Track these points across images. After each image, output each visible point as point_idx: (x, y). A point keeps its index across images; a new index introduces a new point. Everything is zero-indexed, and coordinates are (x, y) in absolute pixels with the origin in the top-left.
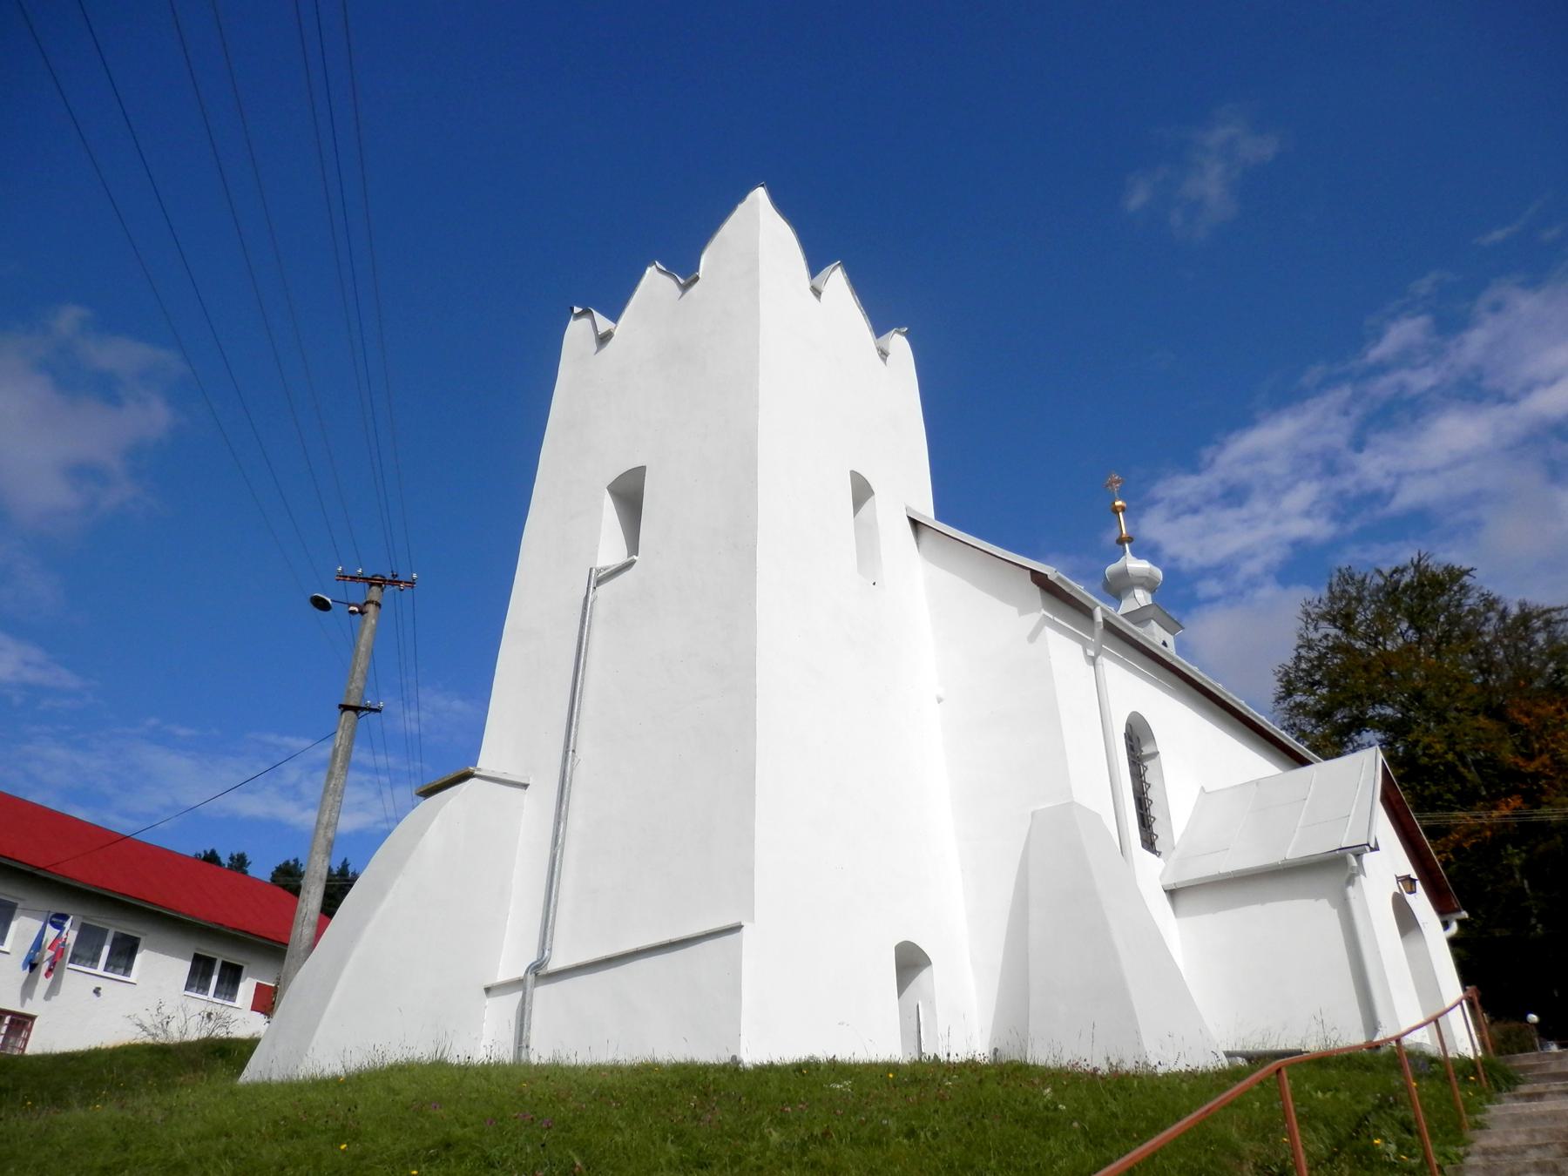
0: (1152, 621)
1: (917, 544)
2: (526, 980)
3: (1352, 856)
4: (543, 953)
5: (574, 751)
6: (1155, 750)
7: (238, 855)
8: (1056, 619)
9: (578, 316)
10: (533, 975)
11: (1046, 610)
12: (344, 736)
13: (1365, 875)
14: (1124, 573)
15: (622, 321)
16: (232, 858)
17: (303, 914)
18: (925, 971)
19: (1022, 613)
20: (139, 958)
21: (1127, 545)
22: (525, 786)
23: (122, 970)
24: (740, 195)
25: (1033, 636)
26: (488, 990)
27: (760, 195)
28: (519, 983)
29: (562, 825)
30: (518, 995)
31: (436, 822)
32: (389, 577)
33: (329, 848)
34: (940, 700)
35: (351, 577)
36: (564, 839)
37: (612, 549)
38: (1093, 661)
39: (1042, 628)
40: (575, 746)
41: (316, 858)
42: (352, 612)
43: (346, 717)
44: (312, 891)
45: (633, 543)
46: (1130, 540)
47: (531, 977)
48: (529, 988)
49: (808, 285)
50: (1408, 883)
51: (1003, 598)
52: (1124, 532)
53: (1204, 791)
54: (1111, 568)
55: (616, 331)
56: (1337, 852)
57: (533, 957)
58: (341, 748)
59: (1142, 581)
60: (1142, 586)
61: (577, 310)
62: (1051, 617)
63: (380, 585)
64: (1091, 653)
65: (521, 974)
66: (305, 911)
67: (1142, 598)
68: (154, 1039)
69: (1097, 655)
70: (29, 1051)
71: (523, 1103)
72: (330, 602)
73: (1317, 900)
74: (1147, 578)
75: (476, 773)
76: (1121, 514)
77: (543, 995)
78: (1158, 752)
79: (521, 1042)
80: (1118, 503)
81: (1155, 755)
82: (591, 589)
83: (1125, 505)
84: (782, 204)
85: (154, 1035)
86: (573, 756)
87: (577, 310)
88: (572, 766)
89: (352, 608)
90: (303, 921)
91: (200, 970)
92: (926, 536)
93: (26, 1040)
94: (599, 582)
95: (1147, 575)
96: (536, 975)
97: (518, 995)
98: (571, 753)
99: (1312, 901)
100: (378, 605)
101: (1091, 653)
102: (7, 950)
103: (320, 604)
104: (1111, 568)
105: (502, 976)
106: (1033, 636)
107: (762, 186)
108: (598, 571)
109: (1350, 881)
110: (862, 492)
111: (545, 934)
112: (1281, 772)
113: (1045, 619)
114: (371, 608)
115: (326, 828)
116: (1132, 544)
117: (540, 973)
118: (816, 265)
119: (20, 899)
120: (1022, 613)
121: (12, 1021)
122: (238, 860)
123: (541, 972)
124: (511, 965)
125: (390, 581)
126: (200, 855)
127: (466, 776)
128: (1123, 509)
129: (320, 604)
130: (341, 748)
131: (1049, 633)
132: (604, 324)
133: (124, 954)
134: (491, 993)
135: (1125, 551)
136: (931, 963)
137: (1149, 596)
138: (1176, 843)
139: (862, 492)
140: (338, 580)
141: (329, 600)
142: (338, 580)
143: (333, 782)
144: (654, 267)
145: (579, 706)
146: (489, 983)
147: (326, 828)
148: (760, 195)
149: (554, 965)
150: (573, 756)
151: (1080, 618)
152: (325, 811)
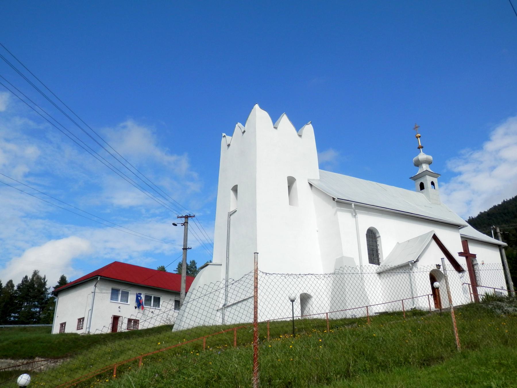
0: (427, 176)
7: (192, 261)
11: (337, 207)
15: (233, 136)
16: (191, 262)
20: (161, 303)
22: (221, 265)
23: (157, 306)
24: (252, 108)
27: (257, 106)
34: (317, 231)
39: (337, 212)
46: (422, 147)
49: (273, 127)
62: (340, 208)
63: (187, 218)
67: (425, 167)
68: (167, 324)
69: (356, 214)
70: (139, 329)
71: (469, 345)
78: (380, 236)
79: (256, 317)
81: (380, 236)
84: (262, 107)
85: (167, 323)
87: (224, 134)
89: (182, 225)
91: (177, 304)
92: (313, 188)
93: (138, 326)
94: (231, 215)
95: (426, 160)
101: (354, 214)
102: (129, 304)
106: (336, 213)
107: (257, 104)
108: (230, 213)
110: (291, 181)
115: (184, 277)
116: (19, 387)
117: (225, 306)
119: (129, 291)
121: (134, 321)
122: (193, 263)
126: (181, 262)
128: (420, 137)
131: (339, 214)
133: (157, 300)
135: (420, 151)
139: (291, 181)
147: (184, 277)
148: (257, 106)
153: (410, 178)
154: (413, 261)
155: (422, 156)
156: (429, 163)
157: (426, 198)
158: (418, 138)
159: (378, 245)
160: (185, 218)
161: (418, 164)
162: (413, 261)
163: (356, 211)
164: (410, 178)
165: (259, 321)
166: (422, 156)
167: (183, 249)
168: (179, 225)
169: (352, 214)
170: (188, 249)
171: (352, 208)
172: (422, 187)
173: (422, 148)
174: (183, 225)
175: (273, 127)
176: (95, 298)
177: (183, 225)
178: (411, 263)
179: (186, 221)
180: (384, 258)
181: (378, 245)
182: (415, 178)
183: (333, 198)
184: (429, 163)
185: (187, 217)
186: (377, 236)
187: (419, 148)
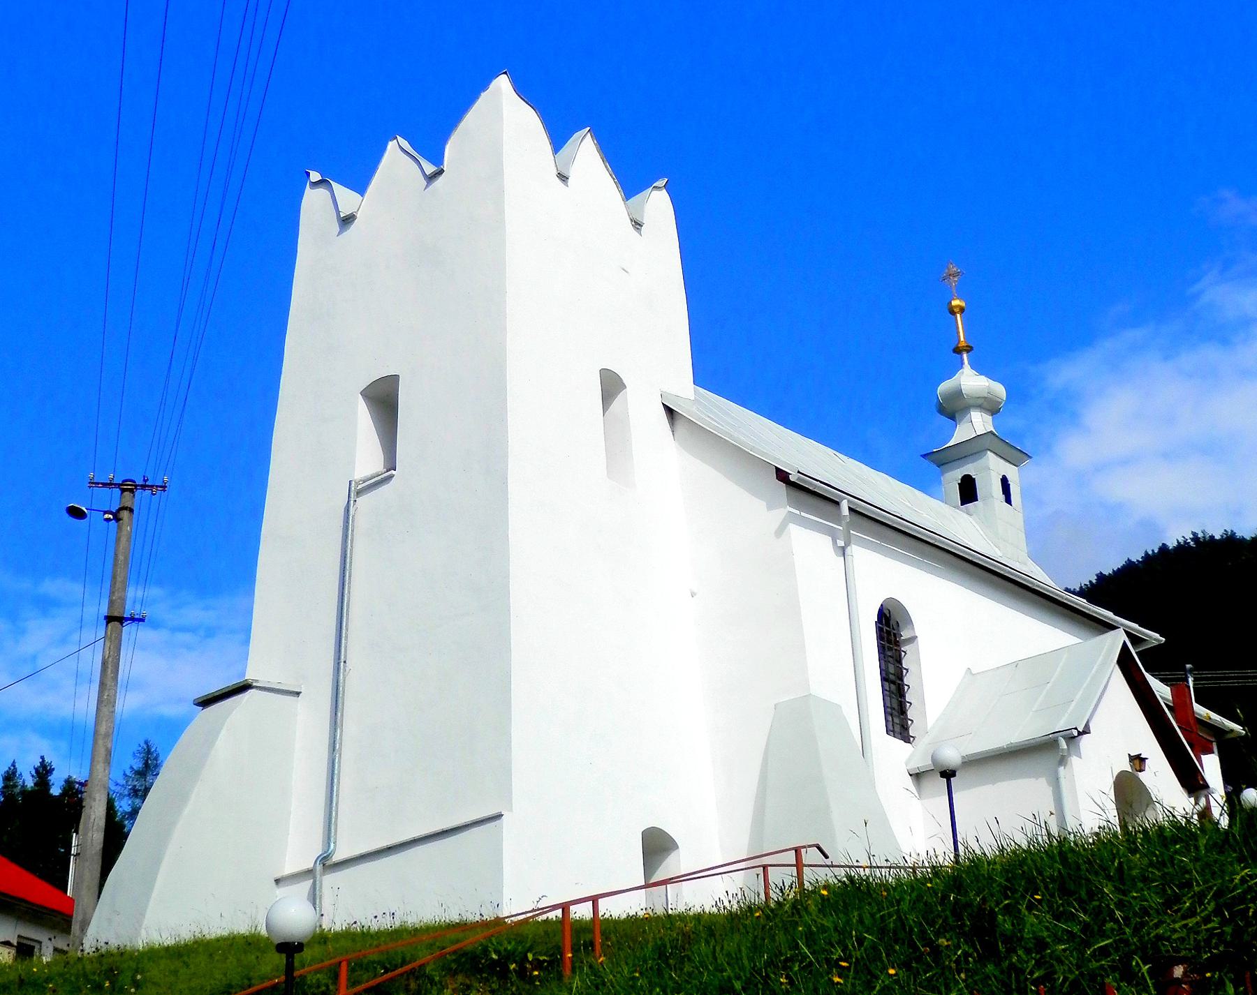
0: (989, 452)
1: (673, 431)
2: (315, 870)
3: (1061, 738)
4: (329, 846)
5: (345, 662)
6: (913, 635)
8: (803, 514)
9: (316, 184)
10: (322, 865)
12: (112, 647)
13: (1141, 754)
14: (958, 394)
15: (366, 195)
17: (92, 820)
18: (672, 854)
19: (770, 508)
21: (965, 356)
22: (298, 694)
25: (780, 531)
26: (277, 881)
27: (502, 84)
28: (309, 873)
29: (338, 731)
30: (309, 883)
31: (223, 732)
32: (140, 482)
33: (108, 756)
35: (102, 484)
36: (341, 744)
37: (368, 460)
38: (843, 551)
40: (345, 657)
41: (98, 767)
42: (108, 520)
43: (112, 629)
44: (98, 798)
45: (391, 464)
46: (969, 349)
47: (319, 867)
48: (318, 876)
50: (1137, 762)
51: (755, 493)
52: (962, 339)
53: (971, 673)
54: (944, 387)
55: (359, 212)
56: (1050, 736)
57: (318, 851)
58: (110, 659)
59: (980, 401)
60: (980, 407)
61: (315, 176)
62: (798, 512)
63: (131, 491)
64: (841, 543)
65: (311, 866)
66: (93, 817)
67: (979, 422)
69: (848, 544)
72: (85, 510)
73: (993, 785)
74: (985, 398)
75: (254, 684)
76: (958, 315)
77: (329, 881)
80: (955, 303)
81: (913, 639)
82: (352, 502)
83: (963, 304)
84: (523, 90)
86: (345, 667)
87: (315, 176)
88: (344, 675)
89: (107, 516)
90: (93, 827)
92: (680, 425)
96: (324, 865)
97: (309, 883)
98: (342, 664)
99: (1033, 780)
100: (131, 510)
101: (841, 543)
103: (76, 513)
104: (944, 387)
105: (288, 870)
106: (780, 531)
107: (505, 73)
108: (357, 484)
109: (1063, 761)
110: (611, 386)
111: (329, 830)
112: (1077, 640)
113: (791, 518)
114: (125, 514)
117: (328, 864)
118: (558, 140)
120: (770, 508)
123: (328, 863)
124: (300, 855)
125: (141, 486)
127: (244, 687)
128: (962, 310)
129: (76, 513)
130: (110, 659)
131: (795, 530)
132: (347, 198)
134: (280, 885)
135: (962, 363)
136: (678, 847)
137: (989, 418)
138: (929, 728)
139: (611, 386)
140: (90, 487)
141: (84, 509)
142: (90, 487)
143: (106, 694)
144: (395, 141)
145: (347, 619)
146: (278, 875)
148: (502, 84)
149: (337, 857)
150: (345, 667)
151: (830, 507)
152: (102, 722)
153: (924, 456)
154: (1076, 729)
155: (970, 380)
156: (991, 407)
157: (979, 529)
158: (953, 313)
159: (907, 670)
160: (123, 491)
161: (953, 409)
162: (1076, 729)
163: (852, 532)
164: (924, 456)
165: (804, 868)
166: (970, 380)
167: (109, 619)
168: (96, 519)
169: (834, 542)
170: (127, 619)
171: (838, 518)
172: (968, 491)
173: (968, 351)
174: (111, 516)
175: (555, 173)
176: (937, 549)
177: (111, 516)
178: (1064, 737)
179: (128, 504)
180: (931, 721)
181: (907, 670)
182: (943, 459)
183: (776, 468)
184: (991, 407)
185: (128, 487)
186: (905, 634)
187: (958, 351)
